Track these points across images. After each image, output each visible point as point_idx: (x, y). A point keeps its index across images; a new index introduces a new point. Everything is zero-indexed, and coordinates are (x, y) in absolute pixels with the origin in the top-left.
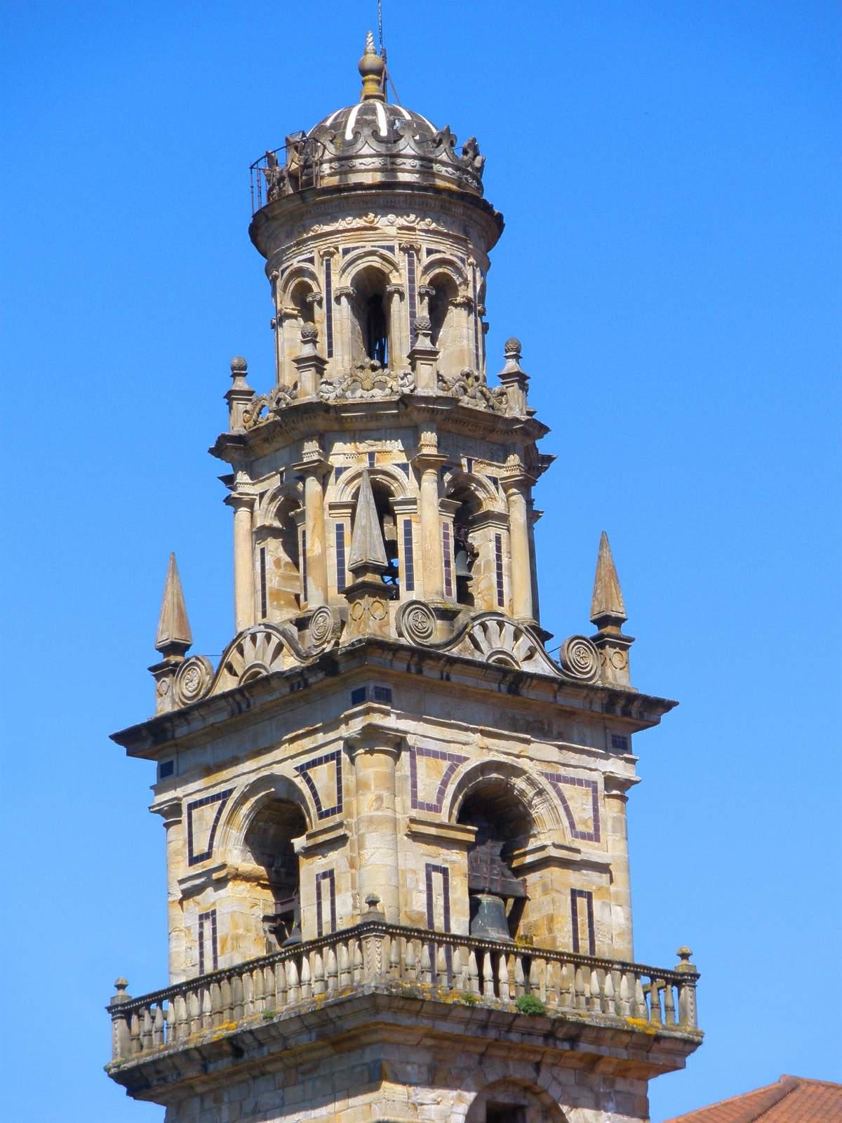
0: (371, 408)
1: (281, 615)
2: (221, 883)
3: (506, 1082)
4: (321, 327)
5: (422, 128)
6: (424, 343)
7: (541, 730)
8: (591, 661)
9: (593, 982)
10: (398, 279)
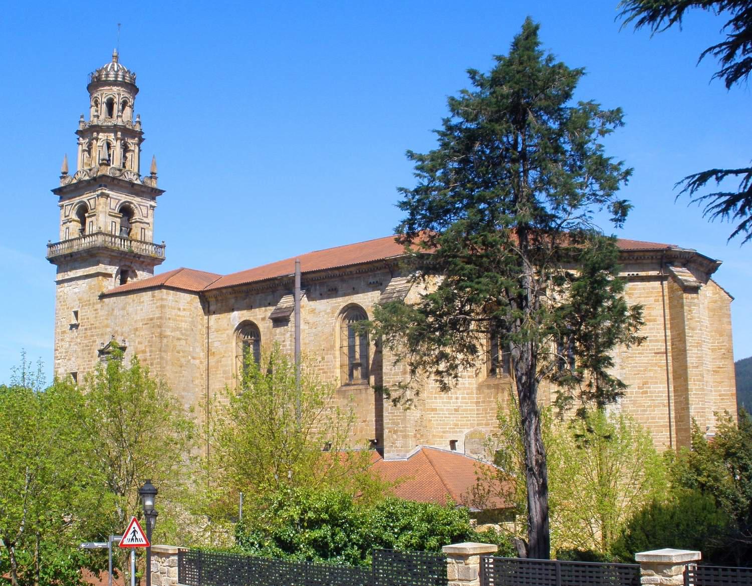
0: (108, 127)
1: (86, 168)
2: (71, 222)
3: (125, 265)
4: (99, 109)
5: (124, 69)
6: (120, 114)
7: (138, 194)
8: (149, 181)
9: (144, 247)
10: (116, 100)
